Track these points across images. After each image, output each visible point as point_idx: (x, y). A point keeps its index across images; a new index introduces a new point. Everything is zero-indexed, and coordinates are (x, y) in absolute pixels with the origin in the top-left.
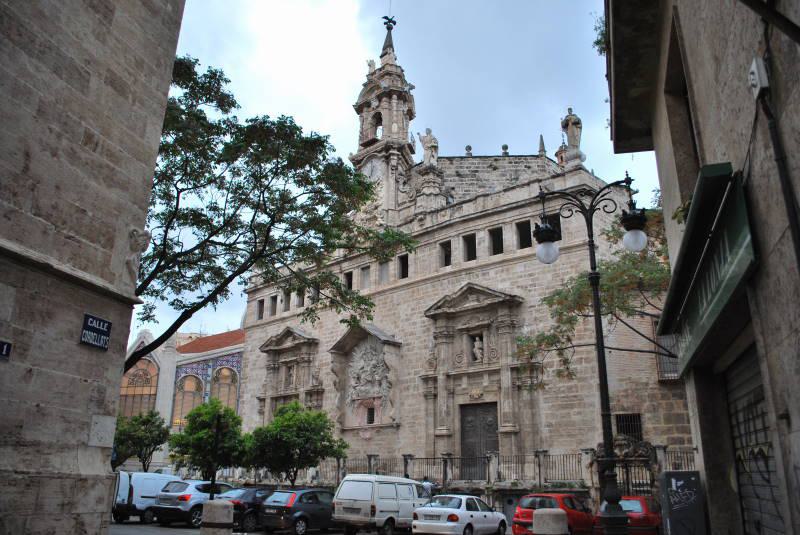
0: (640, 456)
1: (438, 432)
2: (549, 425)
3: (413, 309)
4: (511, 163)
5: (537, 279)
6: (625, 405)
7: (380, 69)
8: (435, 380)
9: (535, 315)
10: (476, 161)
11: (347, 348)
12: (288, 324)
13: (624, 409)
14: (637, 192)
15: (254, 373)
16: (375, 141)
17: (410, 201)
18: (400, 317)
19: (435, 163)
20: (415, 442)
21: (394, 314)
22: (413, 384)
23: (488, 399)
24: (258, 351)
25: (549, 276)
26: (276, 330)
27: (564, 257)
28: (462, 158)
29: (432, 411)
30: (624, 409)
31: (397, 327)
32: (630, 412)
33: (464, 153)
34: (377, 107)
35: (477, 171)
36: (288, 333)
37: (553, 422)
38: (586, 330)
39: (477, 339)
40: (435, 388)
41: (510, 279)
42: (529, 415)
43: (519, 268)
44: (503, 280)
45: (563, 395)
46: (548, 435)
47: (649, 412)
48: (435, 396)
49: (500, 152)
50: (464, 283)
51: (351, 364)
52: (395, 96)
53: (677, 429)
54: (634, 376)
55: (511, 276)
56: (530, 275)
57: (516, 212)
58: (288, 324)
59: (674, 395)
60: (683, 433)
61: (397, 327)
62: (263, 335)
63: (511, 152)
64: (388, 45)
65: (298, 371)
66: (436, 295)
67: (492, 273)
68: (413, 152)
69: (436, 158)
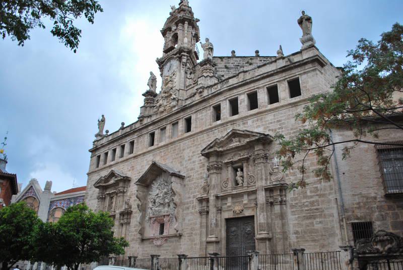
1: (209, 240)
3: (193, 152)
5: (284, 123)
6: (359, 215)
8: (207, 200)
13: (358, 219)
21: (181, 157)
22: (192, 205)
30: (358, 219)
32: (363, 221)
37: (299, 230)
40: (208, 207)
45: (306, 208)
46: (295, 240)
47: (378, 221)
48: (208, 212)
54: (364, 192)
56: (278, 121)
57: (268, 80)
59: (398, 207)
61: (181, 166)
63: (261, 54)
67: (250, 122)
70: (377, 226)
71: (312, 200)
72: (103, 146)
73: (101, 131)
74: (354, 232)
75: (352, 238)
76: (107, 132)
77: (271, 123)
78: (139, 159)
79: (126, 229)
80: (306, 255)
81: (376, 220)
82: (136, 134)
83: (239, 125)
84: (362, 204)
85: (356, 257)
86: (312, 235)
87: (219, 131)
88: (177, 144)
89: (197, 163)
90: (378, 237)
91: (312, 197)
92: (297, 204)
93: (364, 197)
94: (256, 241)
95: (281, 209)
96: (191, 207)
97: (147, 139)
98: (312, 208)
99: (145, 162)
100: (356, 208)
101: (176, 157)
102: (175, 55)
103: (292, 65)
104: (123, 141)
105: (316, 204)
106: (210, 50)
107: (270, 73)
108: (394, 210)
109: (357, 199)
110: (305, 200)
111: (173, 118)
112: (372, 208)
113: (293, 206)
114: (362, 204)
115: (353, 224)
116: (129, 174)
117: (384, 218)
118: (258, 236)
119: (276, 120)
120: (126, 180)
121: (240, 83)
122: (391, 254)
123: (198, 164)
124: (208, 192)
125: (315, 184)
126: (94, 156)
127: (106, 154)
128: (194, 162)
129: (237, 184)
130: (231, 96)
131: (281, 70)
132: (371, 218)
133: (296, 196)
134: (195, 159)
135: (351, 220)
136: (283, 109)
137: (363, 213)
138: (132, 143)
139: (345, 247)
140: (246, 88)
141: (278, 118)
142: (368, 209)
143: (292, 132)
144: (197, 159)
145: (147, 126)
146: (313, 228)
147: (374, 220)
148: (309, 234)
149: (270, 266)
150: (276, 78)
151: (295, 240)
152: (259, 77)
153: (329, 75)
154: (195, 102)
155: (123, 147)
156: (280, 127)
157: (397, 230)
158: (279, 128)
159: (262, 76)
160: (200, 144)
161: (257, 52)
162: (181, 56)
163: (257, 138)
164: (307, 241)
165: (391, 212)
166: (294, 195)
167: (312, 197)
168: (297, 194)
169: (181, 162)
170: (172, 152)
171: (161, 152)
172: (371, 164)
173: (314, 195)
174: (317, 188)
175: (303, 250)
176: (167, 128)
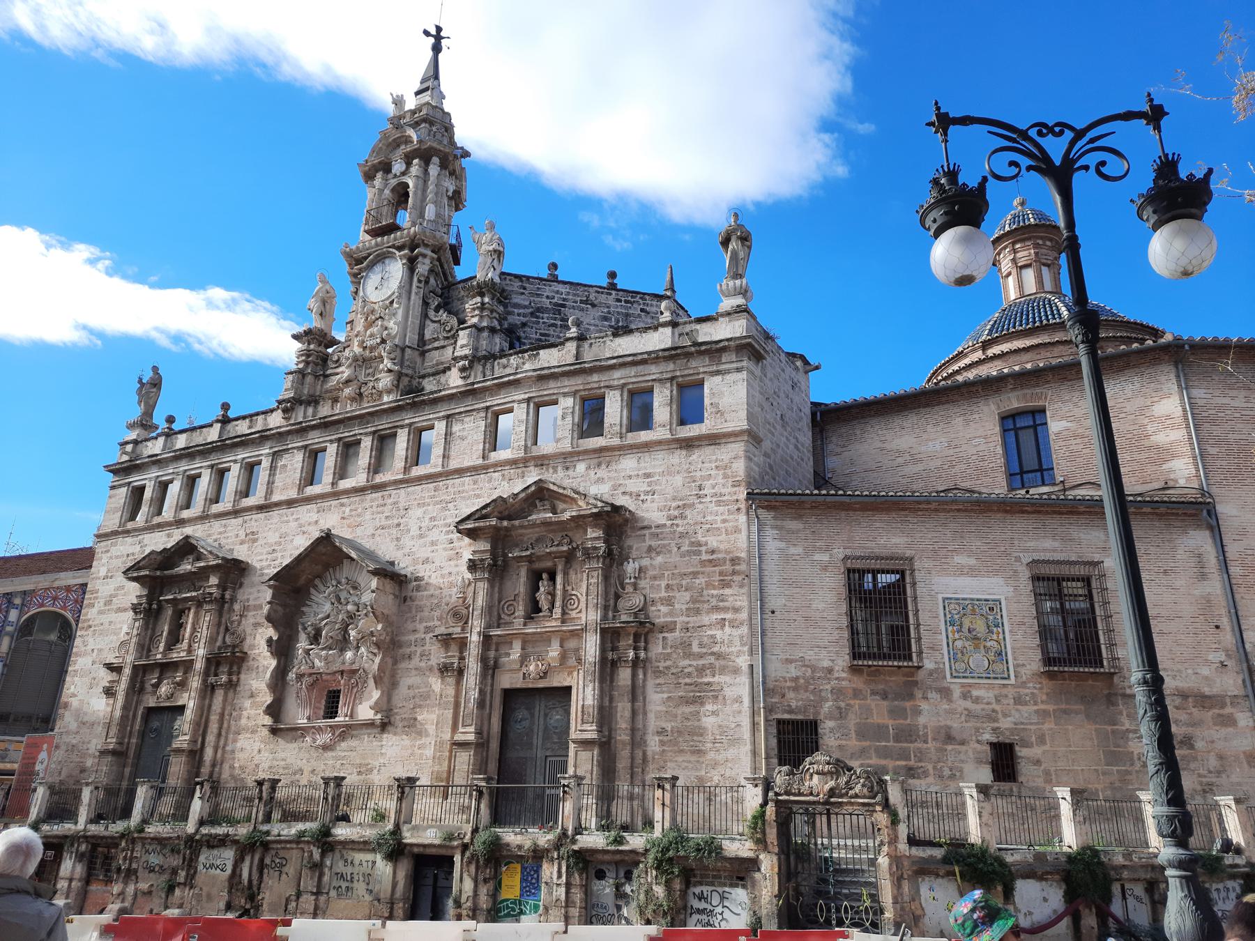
0: (856, 796)
1: (459, 737)
2: (662, 732)
3: (432, 519)
5: (656, 483)
6: (794, 704)
7: (413, 112)
8: (463, 644)
9: (648, 543)
10: (563, 289)
11: (302, 581)
12: (188, 530)
13: (791, 712)
14: (817, 368)
15: (105, 619)
16: (393, 228)
18: (408, 531)
19: (497, 280)
21: (399, 525)
22: (419, 650)
23: (557, 681)
24: (120, 579)
25: (678, 480)
26: (160, 541)
28: (541, 279)
30: (791, 712)
31: (399, 548)
32: (800, 717)
33: (545, 274)
34: (403, 174)
35: (564, 306)
36: (187, 548)
37: (668, 726)
38: (734, 573)
39: (545, 576)
40: (462, 658)
42: (627, 714)
43: (628, 464)
44: (600, 480)
45: (687, 680)
46: (657, 749)
47: (831, 719)
48: (460, 672)
49: (604, 282)
50: (530, 480)
51: (304, 609)
52: (435, 160)
53: (877, 750)
54: (810, 655)
56: (648, 475)
57: (632, 371)
58: (188, 530)
59: (873, 693)
60: (886, 757)
61: (399, 548)
62: (137, 549)
63: (621, 283)
64: (434, 73)
65: (197, 614)
66: (478, 496)
67: (581, 467)
68: (457, 262)
69: (498, 272)
70: (828, 730)
71: (701, 662)
72: (156, 462)
73: (148, 413)
74: (779, 742)
75: (776, 752)
76: (171, 420)
77: (630, 477)
78: (275, 514)
79: (225, 700)
80: (680, 789)
81: (826, 718)
82: (268, 444)
83: (555, 471)
84: (802, 681)
85: (772, 800)
86: (693, 741)
87: (503, 475)
88: (392, 491)
89: (440, 547)
90: (815, 766)
91: (701, 656)
92: (668, 668)
93: (807, 666)
94: (572, 746)
95: (634, 675)
96: (418, 654)
97: (294, 463)
98: (700, 680)
99: (293, 525)
100: (789, 688)
101: (384, 522)
102: (400, 248)
103: (693, 349)
104: (226, 459)
105: (708, 672)
106: (495, 256)
107: (640, 357)
108: (865, 698)
109: (793, 670)
110: (687, 662)
111: (383, 424)
112: (821, 691)
113: (660, 672)
114: (802, 681)
115: (779, 722)
116: (241, 553)
117: (843, 715)
118: (573, 735)
119: (640, 473)
120: (234, 571)
121: (568, 368)
122: (832, 800)
123: (445, 549)
124: (466, 623)
125: (711, 629)
126: (121, 486)
127: (164, 486)
128: (433, 543)
129: (537, 609)
130: (541, 393)
131: (667, 354)
132: (818, 713)
133: (669, 651)
134: (434, 535)
135: (776, 713)
136: (659, 448)
137: (802, 699)
138: (250, 468)
139: (755, 779)
140: (577, 383)
141: (646, 468)
142: (813, 692)
143: (674, 504)
144: (443, 537)
145: (302, 431)
146: (697, 724)
147: (822, 717)
148: (688, 738)
149: (597, 804)
150: (654, 371)
151: (657, 749)
152: (614, 361)
153: (771, 380)
154: (450, 392)
155: (221, 474)
156: (649, 489)
157: (866, 740)
158: (647, 493)
159: (621, 360)
160: (454, 500)
161: (612, 275)
162: (417, 257)
163: (595, 510)
164: (682, 751)
165: (858, 702)
166: (663, 648)
167: (701, 656)
168: (671, 647)
169: (398, 539)
170: (374, 509)
171: (342, 505)
172: (831, 597)
173: (705, 653)
174: (713, 637)
175: (675, 778)
176: (362, 445)
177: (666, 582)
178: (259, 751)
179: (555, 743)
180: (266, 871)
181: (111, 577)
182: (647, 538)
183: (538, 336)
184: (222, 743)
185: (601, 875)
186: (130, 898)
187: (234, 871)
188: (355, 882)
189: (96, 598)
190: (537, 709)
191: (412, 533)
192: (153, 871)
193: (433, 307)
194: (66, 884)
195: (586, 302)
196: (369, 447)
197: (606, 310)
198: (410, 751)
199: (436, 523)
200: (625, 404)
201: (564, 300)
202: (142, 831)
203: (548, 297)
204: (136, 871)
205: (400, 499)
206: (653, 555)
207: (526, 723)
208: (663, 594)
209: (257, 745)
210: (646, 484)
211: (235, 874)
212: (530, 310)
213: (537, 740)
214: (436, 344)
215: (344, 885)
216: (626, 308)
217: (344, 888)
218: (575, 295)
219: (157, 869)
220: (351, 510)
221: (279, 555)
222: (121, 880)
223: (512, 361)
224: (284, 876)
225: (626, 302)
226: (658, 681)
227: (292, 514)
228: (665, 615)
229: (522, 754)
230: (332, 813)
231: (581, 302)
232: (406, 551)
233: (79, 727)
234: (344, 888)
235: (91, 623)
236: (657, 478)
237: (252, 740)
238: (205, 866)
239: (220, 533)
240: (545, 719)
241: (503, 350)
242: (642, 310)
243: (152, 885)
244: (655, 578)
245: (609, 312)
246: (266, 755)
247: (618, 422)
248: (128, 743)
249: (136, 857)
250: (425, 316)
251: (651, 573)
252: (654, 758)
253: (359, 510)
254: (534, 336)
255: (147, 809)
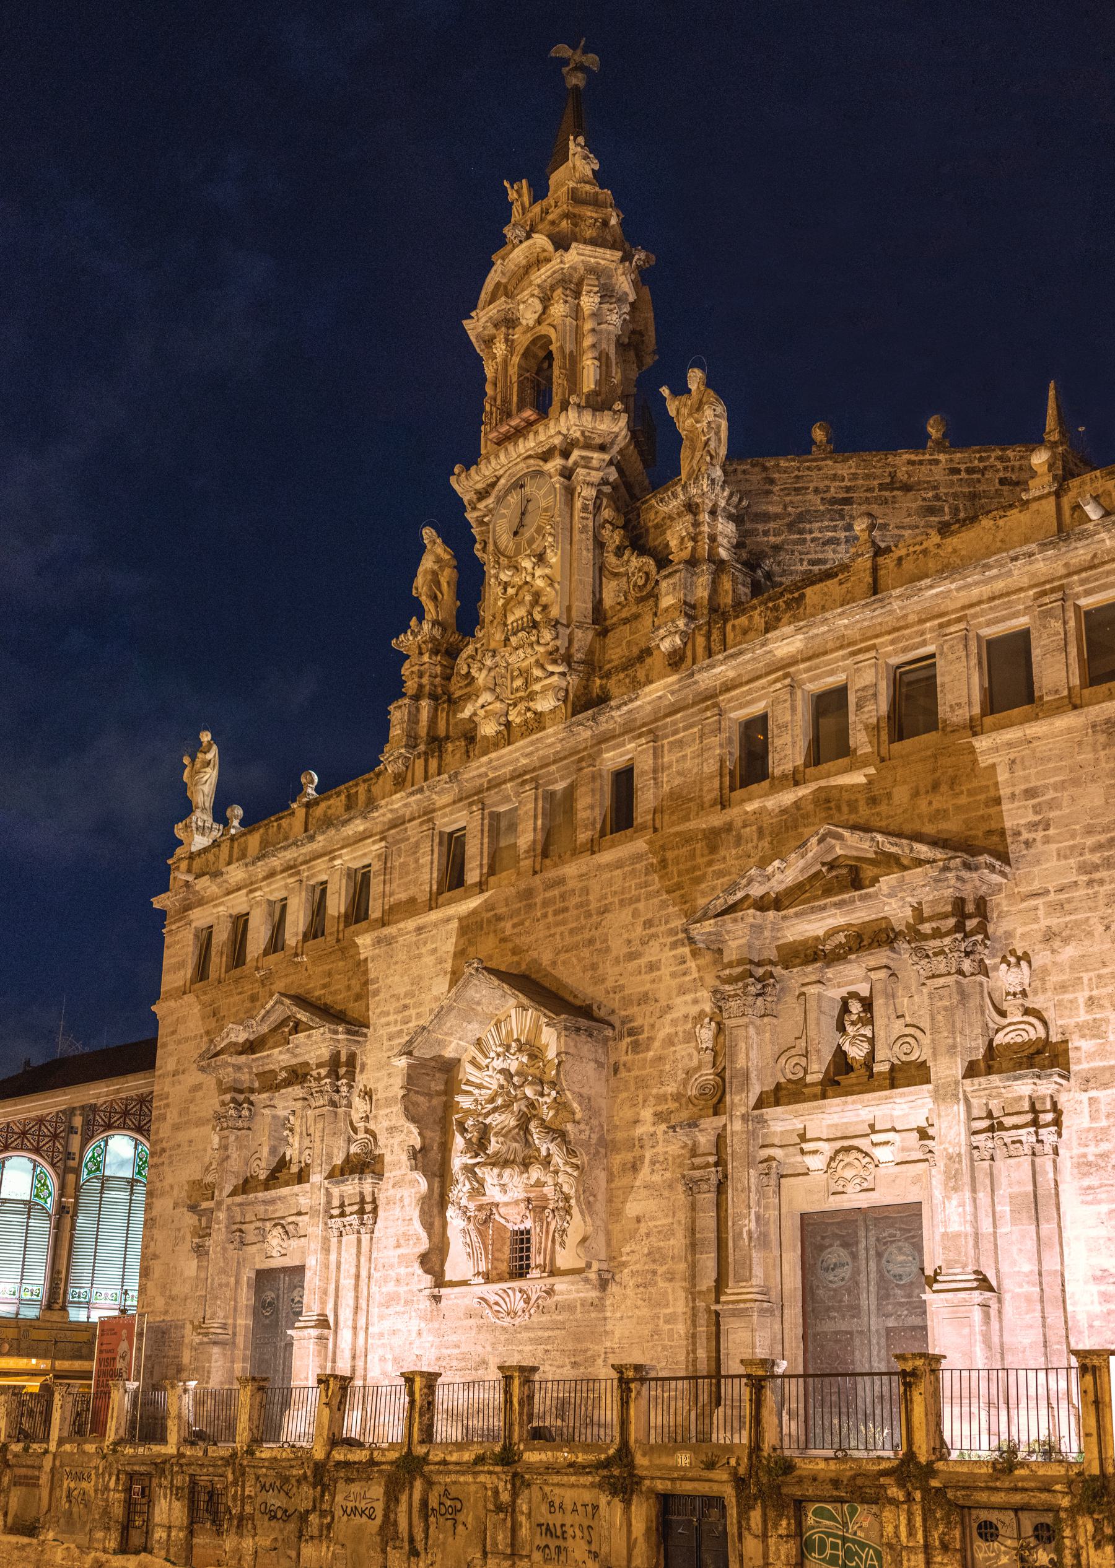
3: (648, 924)
4: (955, 471)
5: (1052, 804)
15: (182, 1136)
17: (640, 600)
18: (608, 950)
20: (656, 1332)
21: (591, 942)
27: (791, 1041)
29: (713, 1236)
35: (847, 501)
41: (958, 808)
55: (963, 800)
56: (1030, 793)
101: (568, 940)
113: (1089, 1164)
123: (674, 975)
128: (652, 967)
133: (1104, 1123)
143: (1090, 841)
156: (1037, 818)
158: (1033, 826)
166: (1093, 1119)
168: (1108, 1116)
169: (594, 967)
170: (550, 918)
177: (1087, 994)
178: (419, 1334)
179: (901, 1304)
180: (432, 1519)
181: (183, 1072)
182: (1041, 913)
183: (805, 567)
184: (362, 1322)
185: (988, 1532)
186: (248, 1558)
187: (386, 1516)
188: (570, 1540)
189: (167, 1105)
190: (862, 1245)
191: (614, 953)
192: (275, 1517)
193: (611, 548)
194: (164, 1535)
195: (889, 486)
196: (532, 813)
197: (930, 494)
198: (650, 1327)
199: (653, 930)
200: (974, 661)
201: (848, 489)
202: (250, 1452)
203: (816, 490)
204: (252, 1517)
205: (591, 898)
206: (1057, 944)
207: (846, 1272)
208: (1083, 1016)
209: (415, 1324)
210: (1030, 811)
211: (389, 1523)
212: (787, 520)
213: (868, 1300)
214: (625, 614)
215: (553, 1543)
216: (970, 483)
217: (552, 1547)
218: (867, 477)
219: (279, 1515)
220: (514, 926)
221: (412, 1012)
222: (234, 1530)
223: (757, 618)
224: (460, 1527)
225: (970, 471)
226: (1086, 1182)
227: (425, 943)
228: (1091, 1056)
229: (843, 1326)
230: (521, 1426)
231: (882, 487)
232: (610, 983)
233: (167, 1304)
234: (552, 1547)
235: (164, 1145)
236: (1051, 795)
237: (406, 1316)
238: (345, 1512)
239: (324, 986)
240: (878, 1263)
241: (740, 603)
242: (1003, 482)
243: (276, 1539)
244: (1063, 987)
245: (937, 498)
246: (431, 1339)
247: (965, 700)
248: (235, 1326)
249: (250, 1497)
250: (601, 570)
251: (1054, 979)
252: (1091, 1326)
253: (527, 924)
254: (799, 568)
255: (256, 1423)
